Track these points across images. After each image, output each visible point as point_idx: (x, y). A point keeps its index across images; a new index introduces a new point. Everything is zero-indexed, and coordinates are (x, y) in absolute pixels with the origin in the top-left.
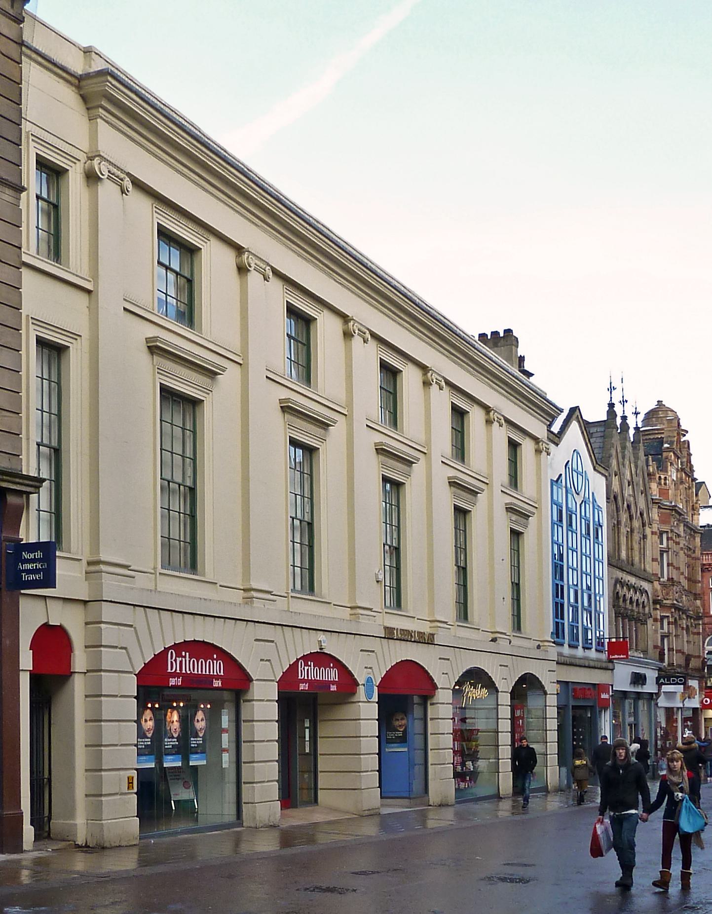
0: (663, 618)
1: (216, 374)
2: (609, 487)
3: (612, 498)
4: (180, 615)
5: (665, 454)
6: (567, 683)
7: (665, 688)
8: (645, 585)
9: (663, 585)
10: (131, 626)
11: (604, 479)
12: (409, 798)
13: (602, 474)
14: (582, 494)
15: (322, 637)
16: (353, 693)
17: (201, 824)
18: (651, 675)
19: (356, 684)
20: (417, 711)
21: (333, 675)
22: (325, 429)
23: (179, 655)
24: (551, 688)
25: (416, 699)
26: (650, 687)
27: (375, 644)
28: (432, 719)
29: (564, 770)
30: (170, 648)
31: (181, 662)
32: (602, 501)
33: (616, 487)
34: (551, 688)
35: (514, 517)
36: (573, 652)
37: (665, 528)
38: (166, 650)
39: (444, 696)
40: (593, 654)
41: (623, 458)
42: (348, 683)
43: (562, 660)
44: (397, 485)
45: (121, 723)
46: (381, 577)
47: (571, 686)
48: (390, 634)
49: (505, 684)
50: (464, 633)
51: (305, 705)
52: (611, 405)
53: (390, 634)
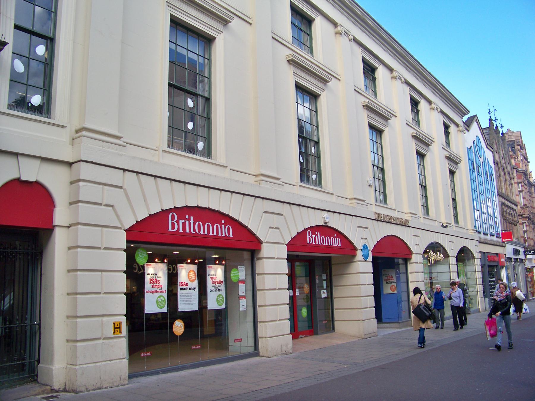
0: (523, 223)
1: (389, 119)
2: (494, 157)
3: (496, 163)
4: (182, 184)
5: (516, 147)
6: (484, 253)
7: (529, 257)
8: (514, 207)
9: (522, 207)
10: (121, 187)
11: (491, 153)
12: (399, 323)
13: (490, 150)
14: (482, 157)
15: (326, 214)
16: (354, 256)
17: (231, 354)
18: (522, 250)
19: (355, 249)
20: (402, 268)
21: (337, 242)
22: (325, 85)
23: (313, 234)
24: (477, 255)
25: (401, 261)
26: (522, 256)
27: (368, 223)
28: (411, 273)
29: (487, 299)
30: (308, 229)
31: (315, 238)
32: (492, 163)
33: (497, 158)
34: (477, 255)
35: (451, 163)
36: (485, 237)
37: (520, 181)
38: (305, 230)
39: (417, 258)
40: (494, 238)
41: (499, 145)
42: (348, 249)
43: (481, 241)
44: (379, 132)
45: (104, 273)
46: (371, 182)
47: (486, 254)
48: (378, 218)
49: (453, 252)
50: (427, 222)
51: (316, 262)
52: (490, 120)
53: (378, 218)
